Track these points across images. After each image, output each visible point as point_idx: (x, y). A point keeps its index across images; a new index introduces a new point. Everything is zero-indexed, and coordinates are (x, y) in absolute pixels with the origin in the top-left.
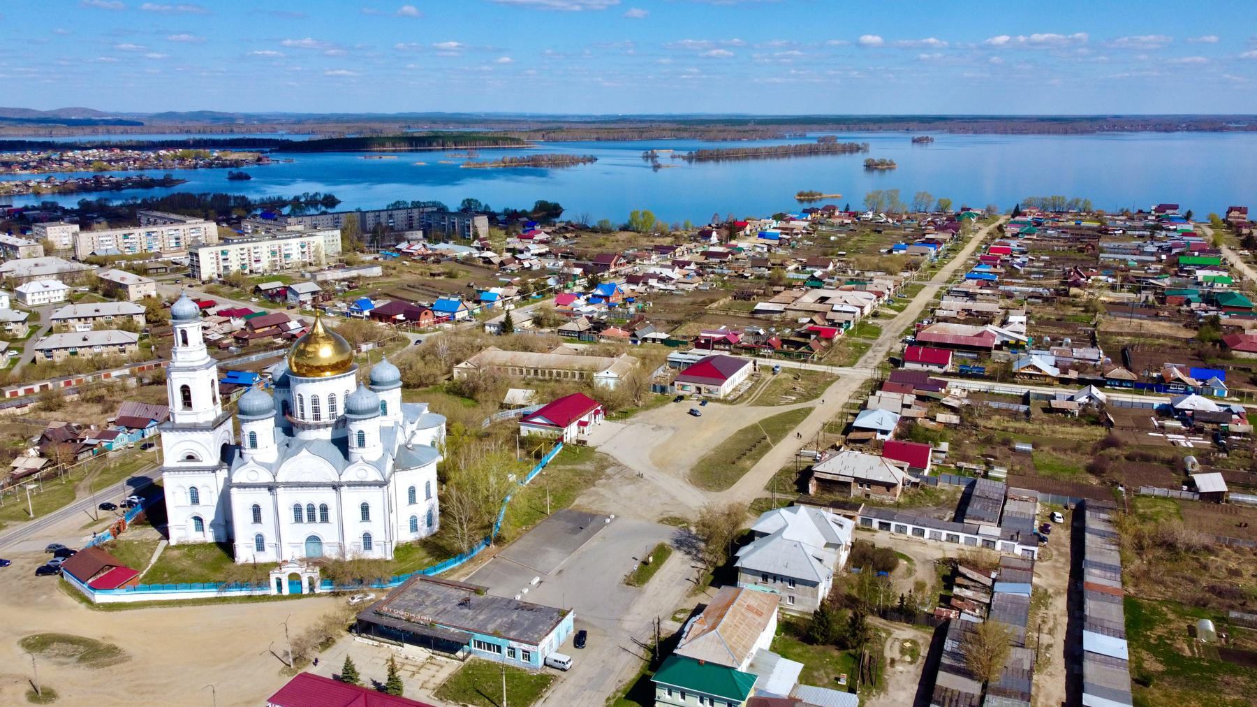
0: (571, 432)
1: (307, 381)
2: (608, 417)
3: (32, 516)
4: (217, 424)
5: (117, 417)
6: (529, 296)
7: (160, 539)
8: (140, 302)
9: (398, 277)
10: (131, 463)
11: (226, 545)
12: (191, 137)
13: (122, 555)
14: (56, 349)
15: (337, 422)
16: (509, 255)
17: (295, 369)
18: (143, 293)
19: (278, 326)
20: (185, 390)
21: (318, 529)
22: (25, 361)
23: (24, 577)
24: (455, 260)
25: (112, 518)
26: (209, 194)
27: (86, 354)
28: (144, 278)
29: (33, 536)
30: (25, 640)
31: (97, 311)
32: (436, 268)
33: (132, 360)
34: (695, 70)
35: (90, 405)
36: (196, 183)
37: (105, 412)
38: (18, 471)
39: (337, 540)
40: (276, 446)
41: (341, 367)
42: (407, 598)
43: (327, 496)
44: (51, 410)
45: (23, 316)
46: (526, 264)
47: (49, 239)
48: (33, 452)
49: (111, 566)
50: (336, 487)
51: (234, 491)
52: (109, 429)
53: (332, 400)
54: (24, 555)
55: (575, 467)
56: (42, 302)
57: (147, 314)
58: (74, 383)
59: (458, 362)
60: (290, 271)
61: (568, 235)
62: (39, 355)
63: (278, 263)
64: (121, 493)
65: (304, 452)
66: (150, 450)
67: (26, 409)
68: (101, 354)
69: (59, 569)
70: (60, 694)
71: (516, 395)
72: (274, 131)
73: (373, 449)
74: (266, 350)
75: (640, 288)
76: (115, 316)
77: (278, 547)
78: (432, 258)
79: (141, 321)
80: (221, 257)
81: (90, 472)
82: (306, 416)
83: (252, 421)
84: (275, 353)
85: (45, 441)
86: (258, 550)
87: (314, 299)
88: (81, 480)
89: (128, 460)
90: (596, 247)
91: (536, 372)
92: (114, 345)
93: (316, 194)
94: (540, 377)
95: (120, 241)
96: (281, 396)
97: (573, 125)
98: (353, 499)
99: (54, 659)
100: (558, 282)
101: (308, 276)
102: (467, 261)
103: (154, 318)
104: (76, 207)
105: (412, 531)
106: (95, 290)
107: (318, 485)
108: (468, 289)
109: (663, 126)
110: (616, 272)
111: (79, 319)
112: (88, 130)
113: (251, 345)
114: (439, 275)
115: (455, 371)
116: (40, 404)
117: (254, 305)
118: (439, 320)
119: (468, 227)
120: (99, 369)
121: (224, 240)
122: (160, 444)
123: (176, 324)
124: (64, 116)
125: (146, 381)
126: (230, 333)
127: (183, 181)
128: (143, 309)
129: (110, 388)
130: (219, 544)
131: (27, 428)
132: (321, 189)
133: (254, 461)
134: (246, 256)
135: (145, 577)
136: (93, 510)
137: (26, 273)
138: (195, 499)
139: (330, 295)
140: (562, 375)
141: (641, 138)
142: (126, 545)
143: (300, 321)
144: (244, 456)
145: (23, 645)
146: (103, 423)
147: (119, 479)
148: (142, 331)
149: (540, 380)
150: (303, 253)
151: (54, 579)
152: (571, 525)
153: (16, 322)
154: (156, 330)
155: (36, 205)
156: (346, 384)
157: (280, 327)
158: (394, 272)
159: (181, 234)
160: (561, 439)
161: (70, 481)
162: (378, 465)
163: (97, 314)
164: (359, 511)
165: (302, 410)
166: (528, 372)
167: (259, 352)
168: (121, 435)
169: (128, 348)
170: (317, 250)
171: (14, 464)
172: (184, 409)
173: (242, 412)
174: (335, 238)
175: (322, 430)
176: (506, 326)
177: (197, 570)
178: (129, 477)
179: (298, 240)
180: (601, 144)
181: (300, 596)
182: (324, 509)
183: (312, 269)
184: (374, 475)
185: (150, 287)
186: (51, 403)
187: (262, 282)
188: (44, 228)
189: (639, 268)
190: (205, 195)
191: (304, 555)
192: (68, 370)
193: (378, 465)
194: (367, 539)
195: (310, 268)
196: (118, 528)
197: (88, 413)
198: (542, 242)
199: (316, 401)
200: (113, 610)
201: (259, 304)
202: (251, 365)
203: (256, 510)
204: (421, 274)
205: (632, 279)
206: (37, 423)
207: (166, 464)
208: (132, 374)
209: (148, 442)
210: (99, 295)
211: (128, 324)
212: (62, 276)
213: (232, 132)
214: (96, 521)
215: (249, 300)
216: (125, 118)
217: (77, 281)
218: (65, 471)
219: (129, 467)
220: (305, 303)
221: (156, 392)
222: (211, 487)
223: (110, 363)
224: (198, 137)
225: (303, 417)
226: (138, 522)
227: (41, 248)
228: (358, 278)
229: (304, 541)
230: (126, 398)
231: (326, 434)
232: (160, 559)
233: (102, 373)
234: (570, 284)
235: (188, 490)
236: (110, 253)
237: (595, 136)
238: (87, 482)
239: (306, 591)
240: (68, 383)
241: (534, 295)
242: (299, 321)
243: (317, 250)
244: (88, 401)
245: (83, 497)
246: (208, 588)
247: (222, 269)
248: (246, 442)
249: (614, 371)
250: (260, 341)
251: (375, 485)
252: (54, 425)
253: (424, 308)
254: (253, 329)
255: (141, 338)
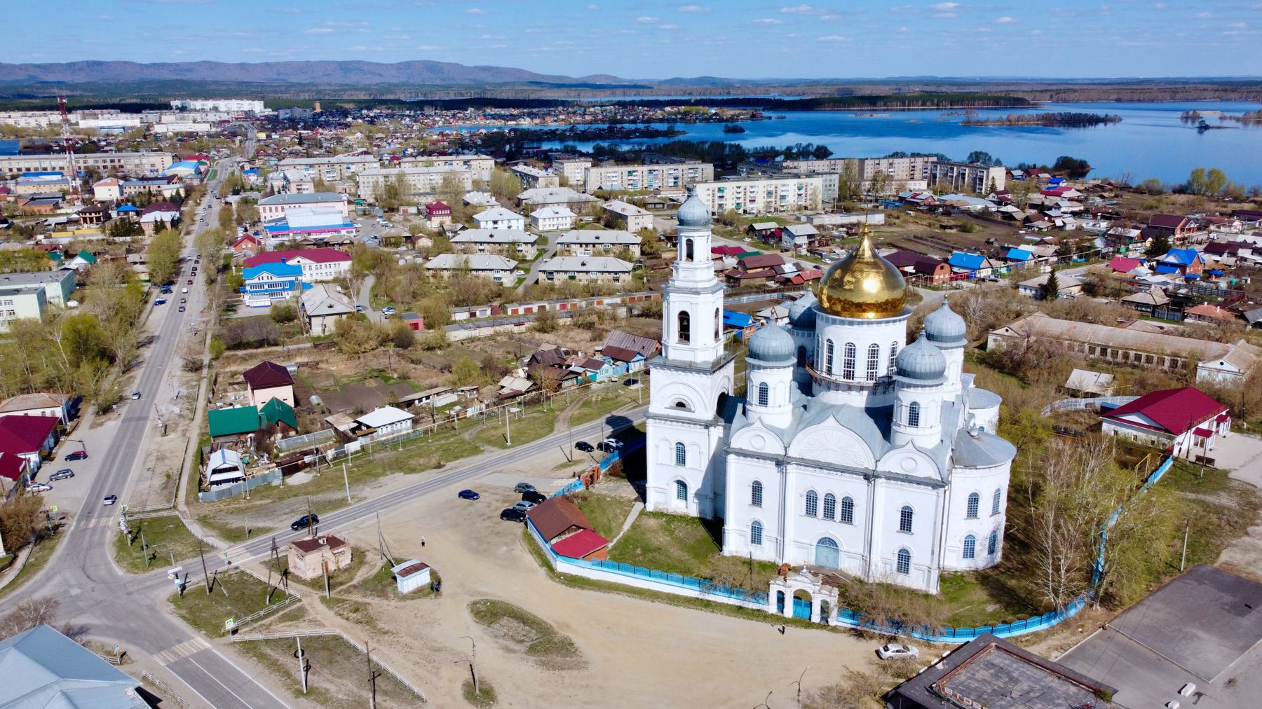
0: (1185, 443)
1: (842, 323)
2: (1237, 428)
3: (509, 444)
4: (717, 366)
5: (604, 347)
6: (1070, 258)
7: (636, 500)
8: (638, 233)
9: (901, 227)
10: (612, 399)
11: (714, 525)
12: (693, 98)
13: (592, 512)
14: (558, 272)
15: (877, 385)
16: (1033, 211)
17: (826, 305)
18: (641, 225)
19: (772, 267)
20: (684, 317)
21: (834, 529)
22: (530, 281)
23: (489, 518)
24: (968, 213)
25: (587, 463)
26: (706, 142)
27: (583, 279)
28: (643, 211)
29: (506, 468)
30: (475, 603)
31: (597, 238)
32: (946, 221)
33: (625, 290)
34: (1242, 25)
35: (580, 330)
36: (694, 133)
37: (594, 339)
38: (505, 391)
39: (860, 550)
40: (791, 406)
41: (889, 309)
42: (979, 676)
43: (855, 488)
44: (545, 332)
45: (533, 238)
46: (1059, 223)
47: (566, 174)
48: (521, 373)
49: (579, 528)
50: (869, 477)
51: (731, 458)
52: (595, 358)
53: (874, 352)
54: (493, 490)
55: (1202, 497)
56: (552, 228)
57: (642, 245)
58: (569, 307)
59: (994, 328)
60: (784, 214)
61: (1106, 194)
62: (542, 277)
63: (773, 205)
64: (599, 432)
65: (831, 421)
66: (633, 387)
67: (523, 328)
68: (596, 280)
69: (524, 516)
70: (500, 697)
71: (1082, 378)
72: (767, 92)
73: (929, 433)
74: (757, 293)
75: (1225, 259)
76: (613, 244)
77: (780, 543)
78: (941, 210)
79: (636, 251)
80: (717, 194)
81: (572, 402)
82: (834, 371)
83: (765, 368)
84: (767, 296)
85: (534, 363)
86: (753, 542)
87: (810, 243)
88: (562, 410)
89: (610, 395)
90: (1145, 209)
91: (1104, 352)
92: (609, 272)
93: (809, 145)
94: (1109, 358)
95: (625, 178)
96: (804, 341)
97: (1085, 87)
98: (889, 498)
99: (501, 641)
100: (1107, 245)
101: (804, 219)
102: (984, 216)
103: (649, 250)
104: (591, 151)
105: (965, 556)
106: (598, 220)
107: (844, 470)
108: (988, 246)
109: (1205, 86)
110: (1184, 239)
111: (581, 245)
112: (608, 92)
113: (742, 285)
114: (951, 227)
115: (991, 338)
116: (536, 324)
117: (747, 245)
118: (955, 277)
119: (981, 180)
120: (593, 295)
121: (717, 178)
122: (647, 382)
123: (682, 231)
124: (591, 82)
125: (636, 312)
126: (722, 271)
127: (684, 133)
128: (639, 240)
129: (601, 315)
130: (703, 520)
131: (521, 347)
132: (816, 141)
133: (762, 422)
134: (741, 195)
135: (615, 548)
136: (569, 447)
137: (541, 201)
138: (681, 459)
139: (827, 241)
140: (1143, 360)
141: (1173, 99)
142: (598, 500)
143: (796, 265)
144: (749, 414)
145: (472, 611)
146: (591, 351)
147: (600, 415)
148: (636, 262)
149: (1109, 363)
150: (800, 195)
151: (516, 527)
152: (1227, 598)
153: (526, 243)
154: (649, 263)
155: (559, 148)
156: (892, 333)
157: (774, 270)
158: (897, 221)
159: (679, 173)
160: (1167, 453)
161: (552, 410)
162: (932, 455)
163: (597, 241)
164: (898, 517)
165: (830, 360)
166: (1092, 350)
167: (750, 293)
168: (606, 366)
169: (622, 276)
170: (814, 194)
171: (502, 383)
172: (680, 342)
173: (753, 355)
174: (832, 183)
175: (854, 393)
176: (1048, 291)
177: (676, 552)
178: (609, 415)
179: (796, 181)
180: (1121, 105)
181: (808, 624)
182: (848, 505)
183: (808, 212)
184: (927, 470)
185: (648, 220)
186: (546, 325)
187: (756, 222)
188: (562, 164)
189: (1221, 235)
190: (703, 143)
191: (812, 561)
192: (565, 294)
193: (932, 455)
194: (904, 560)
195: (805, 211)
196: (592, 477)
197: (578, 339)
198: (1071, 199)
199: (851, 351)
200: (573, 586)
201: (752, 245)
202: (741, 307)
203: (757, 489)
204: (930, 225)
205: (1214, 248)
206: (530, 343)
207: (654, 408)
208: (624, 304)
209: (632, 378)
210: (601, 225)
211: (624, 255)
212: (571, 205)
213: (729, 93)
214: (570, 462)
215: (741, 240)
216: (638, 83)
217: (584, 211)
218: (548, 398)
219: (610, 403)
220: (801, 246)
221: (644, 325)
222: (703, 444)
223: (604, 290)
224: (699, 98)
225: (829, 371)
226: (613, 473)
227: (557, 180)
228: (857, 225)
229: (815, 543)
230: (615, 328)
231: (859, 400)
232: (634, 527)
233: (596, 299)
234: (1123, 248)
235: (674, 447)
236: (615, 188)
237: (1114, 96)
238: (568, 413)
239: (816, 618)
240: (563, 307)
241: (1075, 257)
242: (794, 264)
243: (814, 194)
244: (579, 327)
245: (561, 430)
246: (690, 583)
247: (716, 206)
248: (754, 395)
249: (1231, 362)
250: (752, 282)
251: (927, 484)
252: (545, 347)
253: (937, 263)
254: (746, 269)
255: (634, 269)
